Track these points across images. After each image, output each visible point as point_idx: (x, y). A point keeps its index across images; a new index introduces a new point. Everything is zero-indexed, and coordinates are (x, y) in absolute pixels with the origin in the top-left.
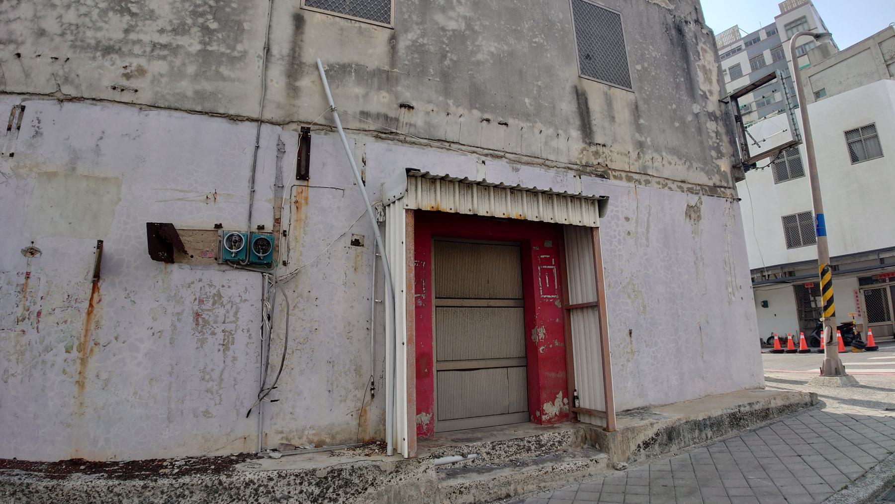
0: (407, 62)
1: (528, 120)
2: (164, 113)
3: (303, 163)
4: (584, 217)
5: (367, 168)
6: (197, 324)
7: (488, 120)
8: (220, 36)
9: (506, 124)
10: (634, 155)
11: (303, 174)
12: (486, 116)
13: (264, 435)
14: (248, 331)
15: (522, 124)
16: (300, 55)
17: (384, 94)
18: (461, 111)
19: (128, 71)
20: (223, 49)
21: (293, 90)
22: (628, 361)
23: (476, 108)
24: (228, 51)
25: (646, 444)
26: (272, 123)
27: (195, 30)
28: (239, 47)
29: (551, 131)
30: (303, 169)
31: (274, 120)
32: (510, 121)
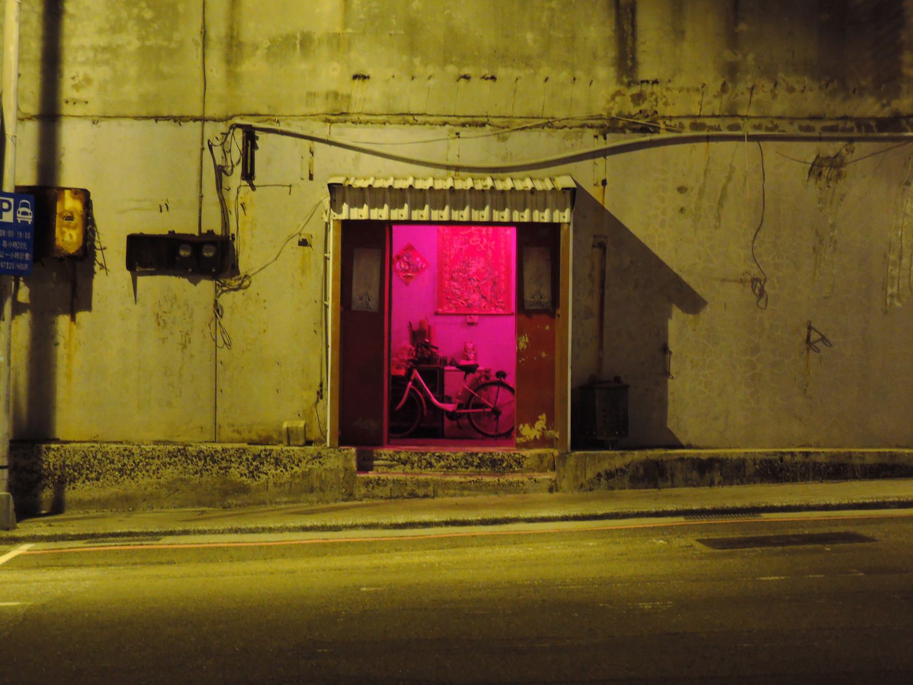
0: (362, 16)
1: (527, 65)
2: (114, 122)
5: (315, 158)
6: (159, 324)
7: (466, 77)
8: (156, 26)
9: (493, 78)
10: (714, 86)
11: (248, 175)
12: (466, 71)
15: (517, 73)
16: (238, 34)
17: (335, 65)
18: (430, 70)
19: (77, 81)
20: (161, 42)
21: (233, 77)
23: (452, 63)
24: (166, 43)
26: (215, 120)
27: (131, 24)
28: (176, 36)
29: (564, 75)
31: (217, 117)
32: (501, 72)
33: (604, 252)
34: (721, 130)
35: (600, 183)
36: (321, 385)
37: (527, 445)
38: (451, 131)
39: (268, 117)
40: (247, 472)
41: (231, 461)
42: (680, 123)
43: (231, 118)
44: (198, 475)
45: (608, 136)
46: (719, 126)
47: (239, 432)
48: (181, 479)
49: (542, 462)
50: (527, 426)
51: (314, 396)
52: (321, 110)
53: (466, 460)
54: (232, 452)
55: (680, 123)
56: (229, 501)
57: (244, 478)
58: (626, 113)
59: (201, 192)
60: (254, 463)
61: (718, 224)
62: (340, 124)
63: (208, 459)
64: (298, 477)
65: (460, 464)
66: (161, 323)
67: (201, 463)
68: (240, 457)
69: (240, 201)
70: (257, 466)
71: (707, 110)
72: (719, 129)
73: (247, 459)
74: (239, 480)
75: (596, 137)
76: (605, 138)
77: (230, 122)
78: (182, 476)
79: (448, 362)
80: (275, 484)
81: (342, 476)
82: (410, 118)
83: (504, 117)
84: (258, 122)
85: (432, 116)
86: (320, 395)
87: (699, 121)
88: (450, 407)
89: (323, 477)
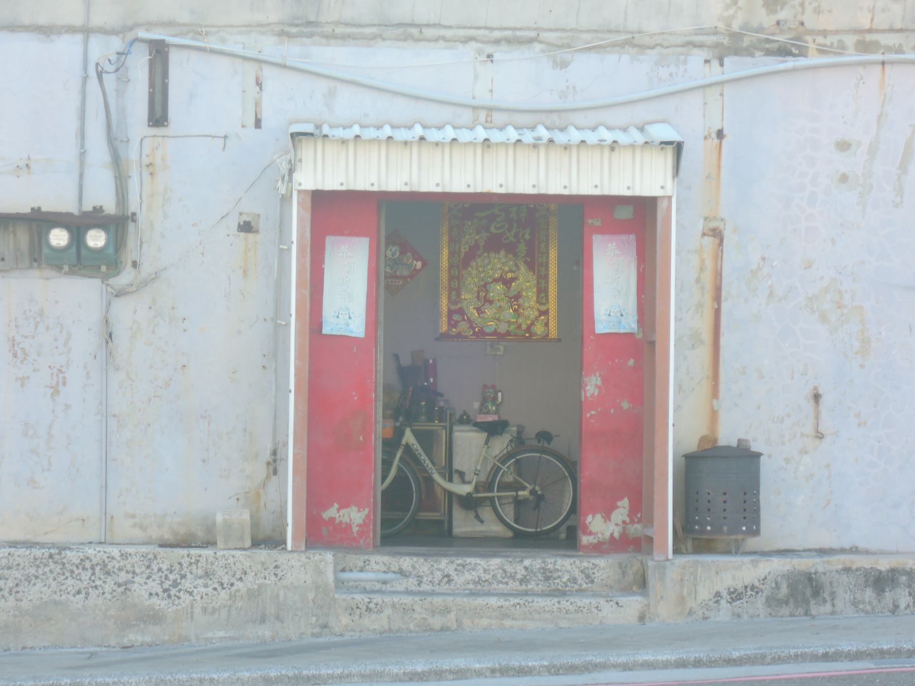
3: (158, 98)
4: (647, 177)
6: (15, 356)
11: (158, 117)
13: (109, 518)
14: (85, 368)
22: (804, 451)
25: (735, 595)
30: (158, 108)
33: (721, 241)
34: (903, 53)
35: (714, 135)
36: (274, 453)
37: (599, 549)
38: (479, 52)
39: (196, 30)
40: (160, 590)
41: (134, 573)
42: (840, 41)
43: (131, 29)
44: (82, 596)
45: (726, 60)
46: (900, 45)
47: (142, 527)
48: (56, 603)
49: (624, 573)
50: (599, 517)
51: (261, 471)
52: (273, 18)
53: (505, 571)
54: (135, 559)
55: (840, 41)
56: (132, 637)
57: (155, 600)
58: (755, 25)
59: (82, 146)
60: (172, 577)
61: (898, 200)
62: (305, 39)
63: (98, 568)
64: (242, 597)
65: (494, 576)
66: (20, 354)
67: (86, 576)
68: (148, 567)
69: (146, 161)
70: (175, 581)
71: (881, 21)
72: (899, 50)
73: (160, 570)
74: (147, 603)
75: (707, 61)
76: (722, 65)
77: (130, 36)
78: (56, 597)
79: (457, 416)
80: (204, 610)
81: (311, 596)
82: (414, 31)
83: (563, 30)
84: (175, 36)
85: (450, 27)
86: (274, 465)
87: (869, 37)
88: (464, 489)
89: (281, 598)
